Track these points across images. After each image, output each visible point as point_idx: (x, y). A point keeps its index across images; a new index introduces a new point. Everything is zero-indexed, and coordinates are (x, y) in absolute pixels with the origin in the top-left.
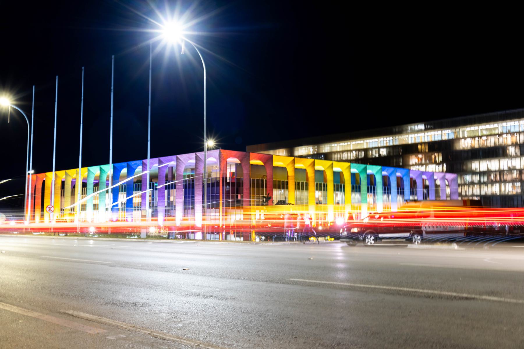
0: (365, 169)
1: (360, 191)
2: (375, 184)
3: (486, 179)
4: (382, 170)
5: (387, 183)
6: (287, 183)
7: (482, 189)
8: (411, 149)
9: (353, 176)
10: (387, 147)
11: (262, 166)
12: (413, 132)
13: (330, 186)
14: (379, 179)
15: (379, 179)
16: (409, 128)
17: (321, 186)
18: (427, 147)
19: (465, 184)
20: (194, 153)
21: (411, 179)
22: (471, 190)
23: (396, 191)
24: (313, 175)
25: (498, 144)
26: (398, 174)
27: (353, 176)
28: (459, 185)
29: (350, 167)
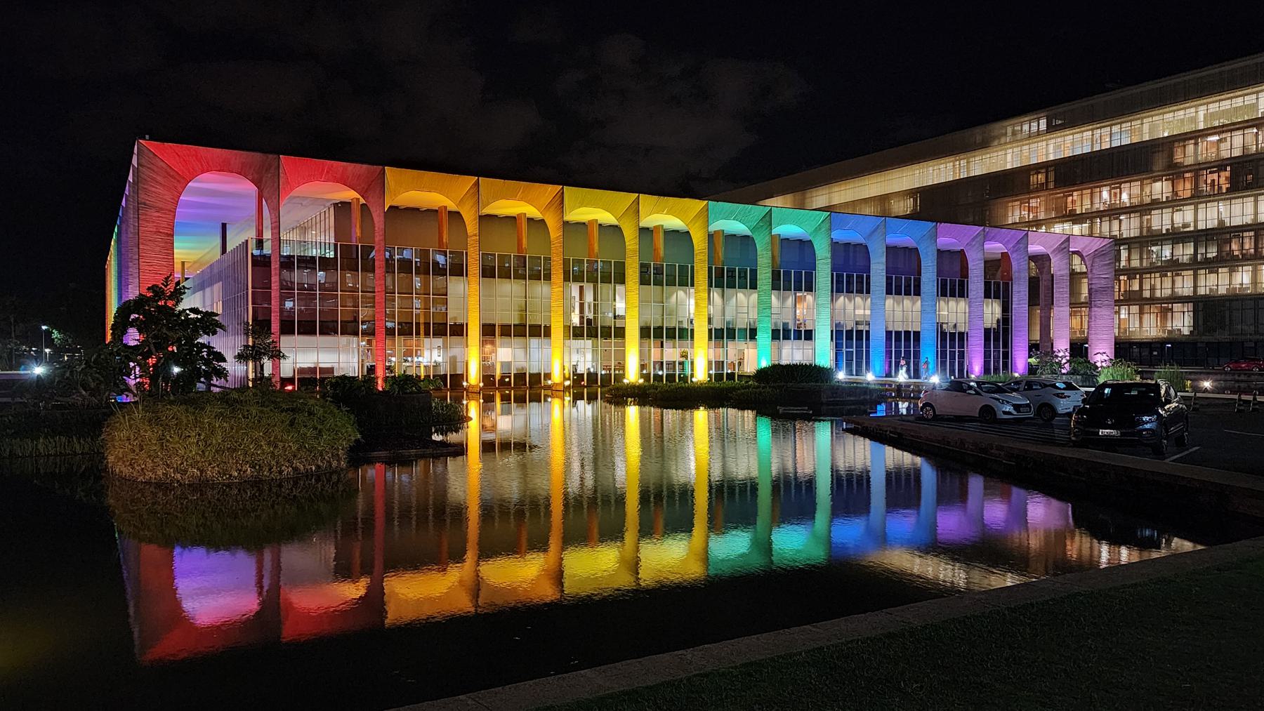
3: (1212, 253)
7: (1201, 282)
8: (1011, 184)
10: (912, 193)
12: (1016, 139)
13: (976, 283)
16: (1009, 130)
17: (787, 280)
18: (1052, 176)
19: (1152, 269)
22: (1167, 282)
23: (637, 280)
28: (1119, 272)
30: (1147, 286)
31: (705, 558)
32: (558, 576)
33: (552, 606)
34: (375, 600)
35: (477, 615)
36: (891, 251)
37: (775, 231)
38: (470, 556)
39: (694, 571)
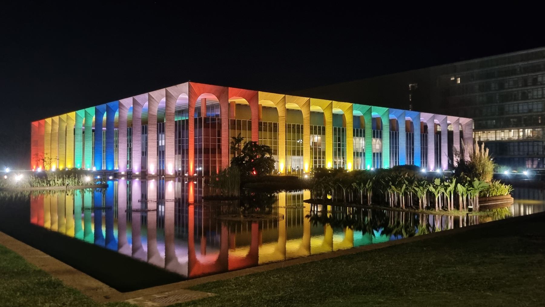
0: (370, 111)
1: (364, 136)
2: (398, 130)
4: (389, 113)
5: (396, 128)
6: (324, 129)
7: (498, 136)
9: (357, 119)
11: (246, 105)
13: (369, 131)
14: (385, 123)
15: (385, 123)
20: (165, 89)
21: (422, 123)
24: (309, 115)
25: (540, 192)
26: (408, 118)
27: (357, 119)
29: (352, 108)
30: (477, 137)
31: (284, 252)
32: (309, 247)
33: (328, 254)
34: (253, 256)
35: (353, 248)
36: (407, 122)
37: (230, 101)
38: (281, 240)
39: (349, 245)
